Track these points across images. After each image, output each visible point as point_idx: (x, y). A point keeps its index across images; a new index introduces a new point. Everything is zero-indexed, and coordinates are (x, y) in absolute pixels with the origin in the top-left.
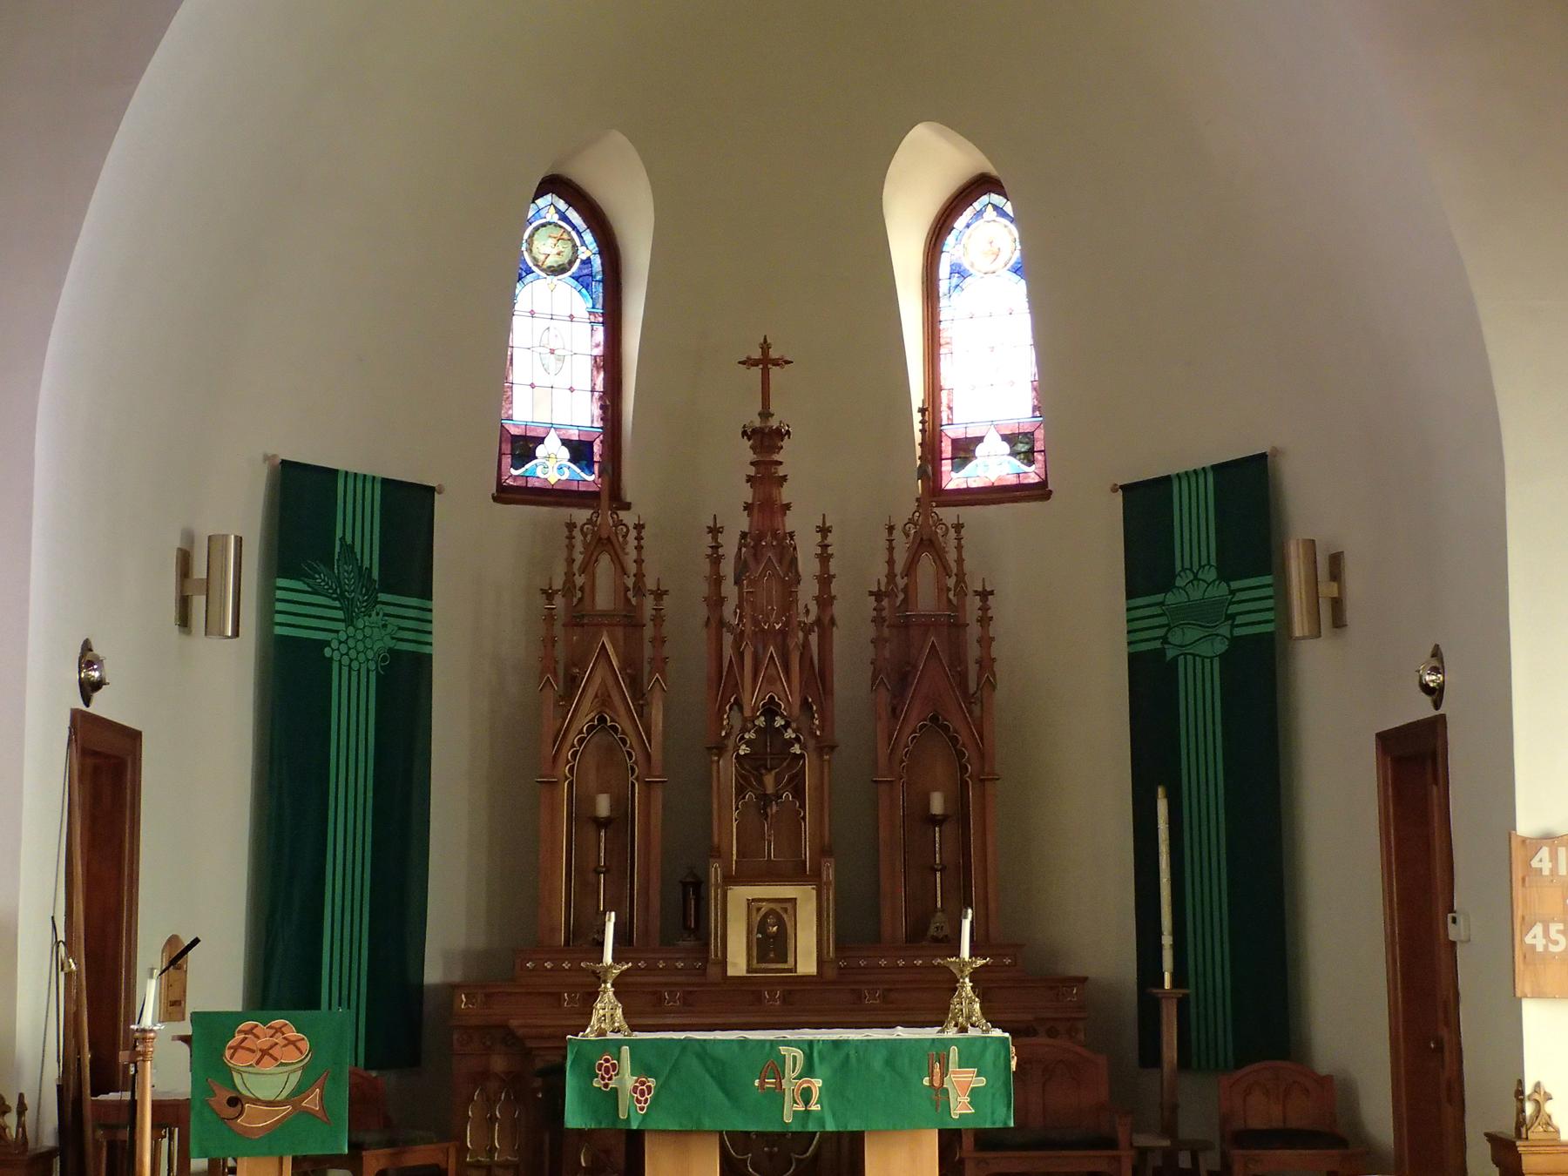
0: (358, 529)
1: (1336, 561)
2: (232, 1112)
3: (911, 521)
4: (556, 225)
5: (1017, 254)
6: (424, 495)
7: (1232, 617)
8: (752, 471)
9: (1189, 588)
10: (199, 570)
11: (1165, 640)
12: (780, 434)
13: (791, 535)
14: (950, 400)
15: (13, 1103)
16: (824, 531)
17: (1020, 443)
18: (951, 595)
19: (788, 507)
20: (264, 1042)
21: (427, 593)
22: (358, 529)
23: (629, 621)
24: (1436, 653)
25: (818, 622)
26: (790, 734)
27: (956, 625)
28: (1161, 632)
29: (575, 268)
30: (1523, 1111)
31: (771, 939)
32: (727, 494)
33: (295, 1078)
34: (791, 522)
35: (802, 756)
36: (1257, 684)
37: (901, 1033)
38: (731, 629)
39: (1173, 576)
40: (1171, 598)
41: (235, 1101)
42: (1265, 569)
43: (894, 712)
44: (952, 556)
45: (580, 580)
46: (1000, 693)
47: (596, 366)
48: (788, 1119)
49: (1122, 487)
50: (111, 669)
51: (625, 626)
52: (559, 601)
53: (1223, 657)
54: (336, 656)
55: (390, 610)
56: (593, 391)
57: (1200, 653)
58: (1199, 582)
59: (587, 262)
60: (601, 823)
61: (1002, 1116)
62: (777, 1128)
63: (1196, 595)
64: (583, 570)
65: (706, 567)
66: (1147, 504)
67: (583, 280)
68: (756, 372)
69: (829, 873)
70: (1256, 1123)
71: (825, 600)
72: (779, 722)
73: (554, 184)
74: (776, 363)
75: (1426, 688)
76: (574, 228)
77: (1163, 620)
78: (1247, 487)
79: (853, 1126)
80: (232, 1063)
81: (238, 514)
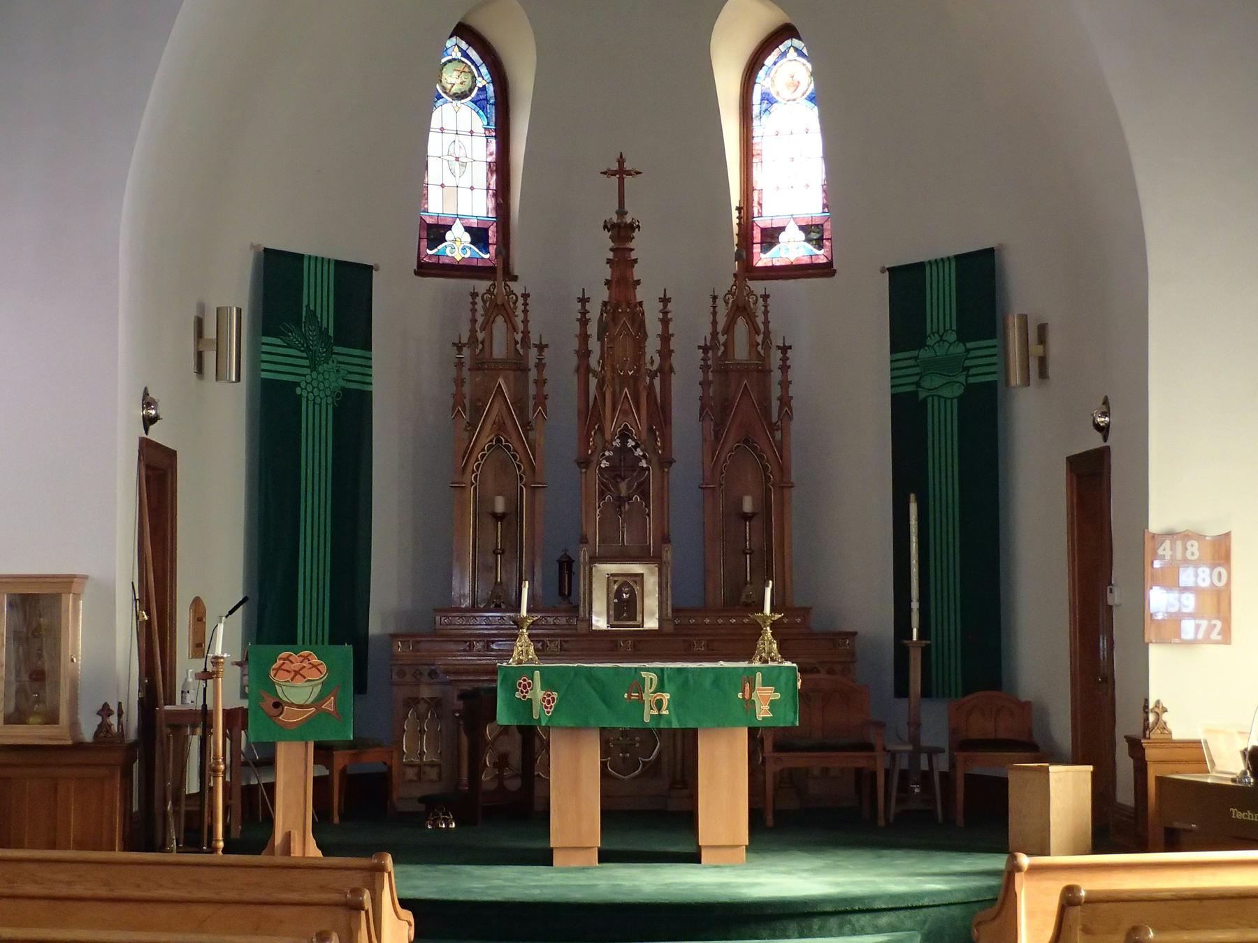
0: (318, 298)
1: (1042, 329)
2: (274, 711)
3: (730, 292)
4: (460, 61)
5: (812, 86)
6: (365, 272)
7: (968, 369)
8: (611, 255)
9: (936, 347)
10: (210, 332)
11: (918, 384)
12: (632, 227)
13: (641, 304)
14: (760, 199)
15: (114, 707)
16: (665, 300)
17: (813, 232)
18: (759, 348)
19: (638, 282)
20: (296, 665)
21: (367, 346)
22: (318, 298)
23: (518, 366)
24: (1106, 402)
25: (661, 369)
26: (639, 452)
27: (764, 371)
28: (915, 379)
29: (474, 94)
30: (1147, 719)
31: (625, 604)
32: (592, 274)
33: (317, 690)
34: (640, 294)
35: (648, 469)
36: (983, 415)
37: (722, 664)
38: (595, 374)
39: (925, 337)
40: (924, 354)
41: (278, 705)
42: (992, 335)
43: (717, 438)
44: (760, 319)
45: (480, 336)
46: (795, 426)
47: (490, 169)
48: (647, 720)
49: (889, 269)
50: (163, 410)
51: (515, 370)
52: (466, 352)
53: (960, 398)
54: (305, 394)
55: (341, 358)
56: (488, 189)
57: (944, 393)
58: (942, 338)
59: (483, 89)
60: (497, 517)
61: (791, 718)
62: (640, 726)
63: (940, 351)
64: (483, 329)
65: (577, 327)
66: (907, 282)
67: (480, 103)
68: (615, 179)
69: (668, 555)
70: (975, 735)
71: (666, 353)
72: (631, 443)
73: (464, 31)
74: (629, 173)
75: (1097, 427)
76: (473, 62)
77: (917, 370)
78: (979, 273)
79: (691, 725)
80: (276, 679)
81: (234, 290)
